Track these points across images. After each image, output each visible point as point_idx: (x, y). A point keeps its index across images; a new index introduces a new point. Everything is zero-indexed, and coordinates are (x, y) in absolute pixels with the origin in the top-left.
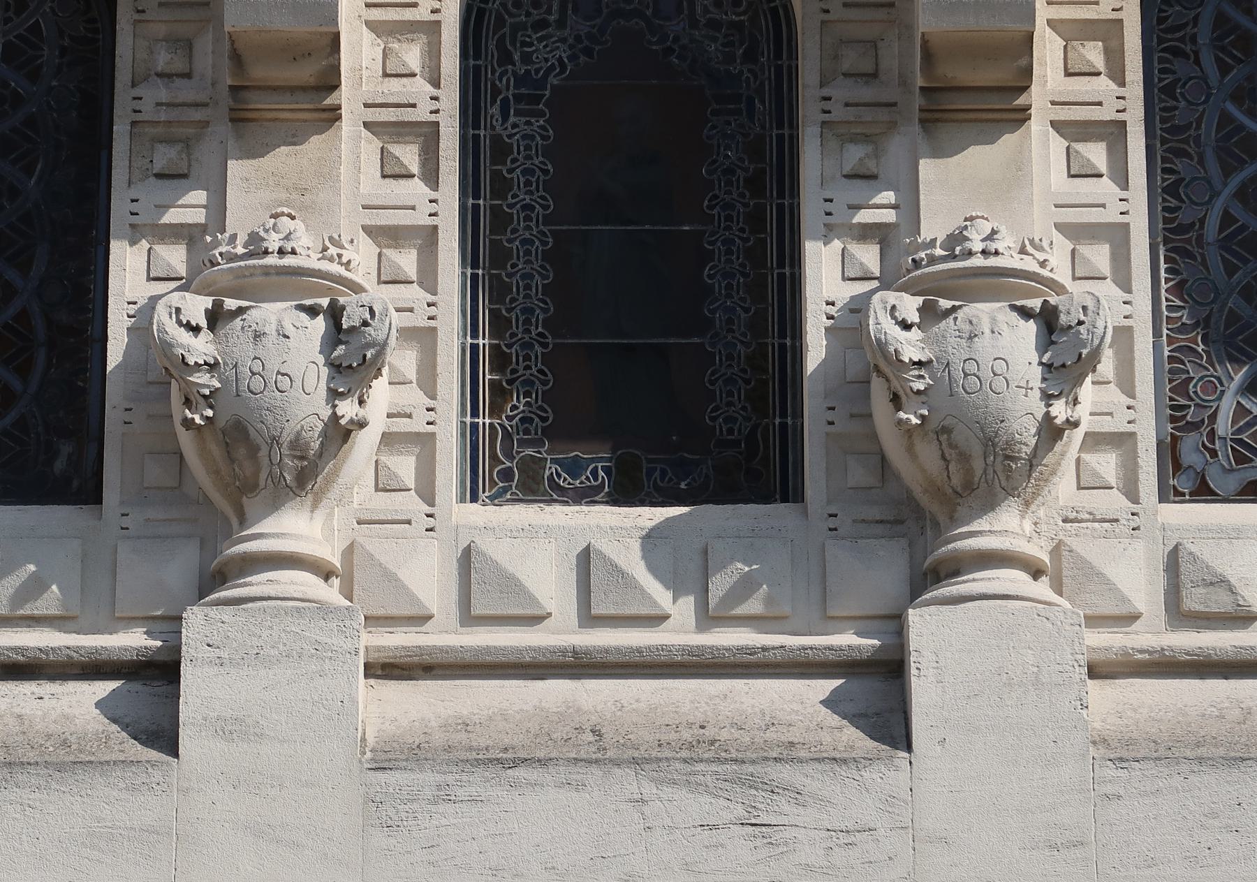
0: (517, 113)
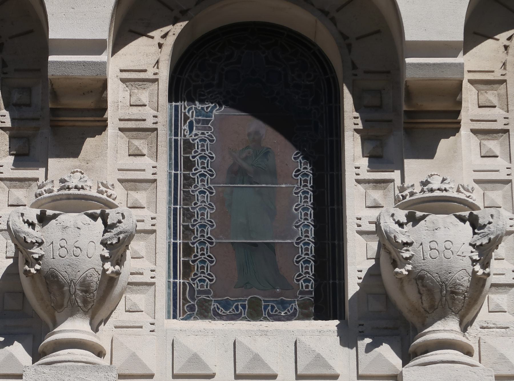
0: (197, 129)
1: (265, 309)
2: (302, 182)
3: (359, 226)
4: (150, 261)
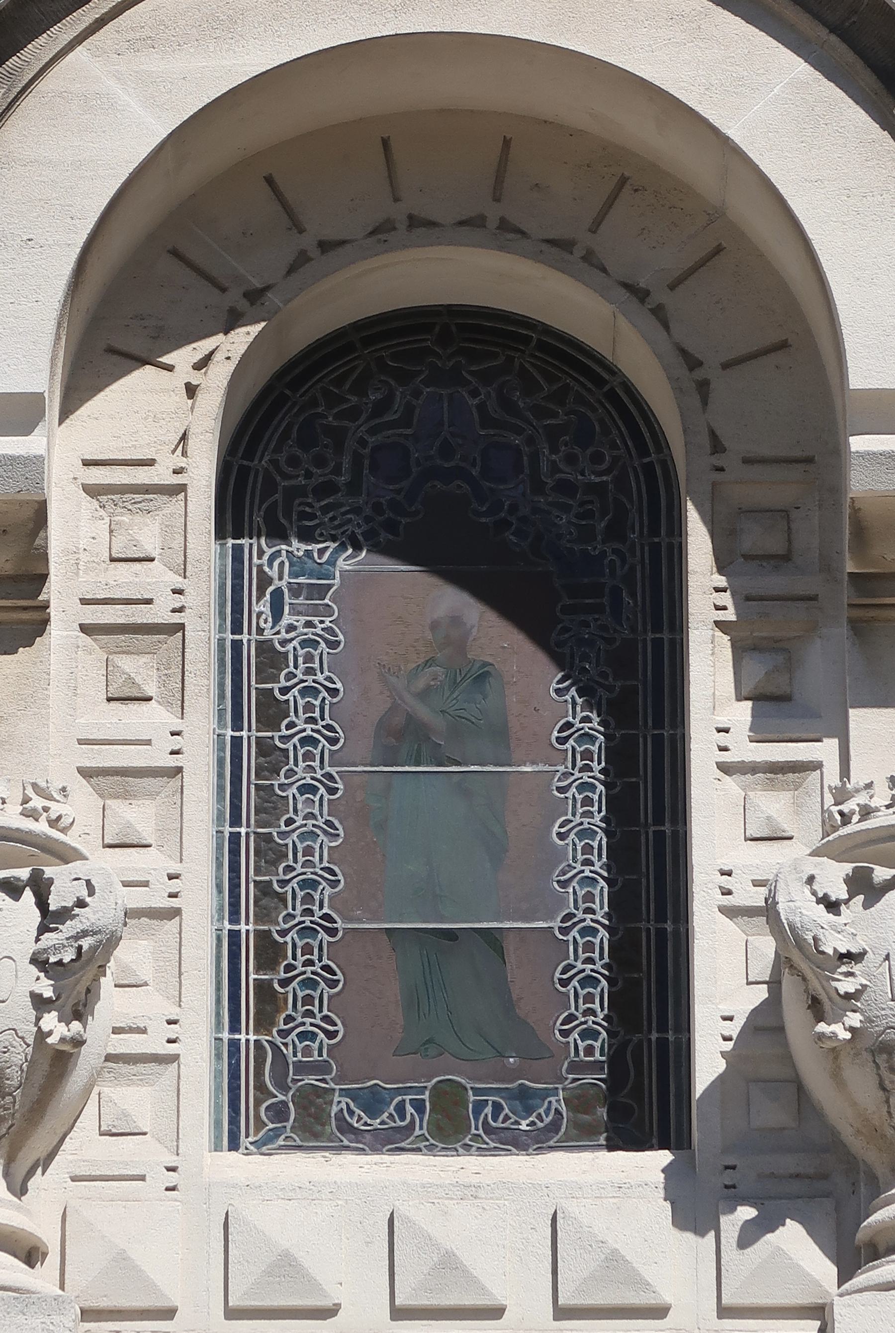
0: (295, 611)
1: (477, 1112)
2: (578, 757)
3: (727, 892)
4: (167, 994)
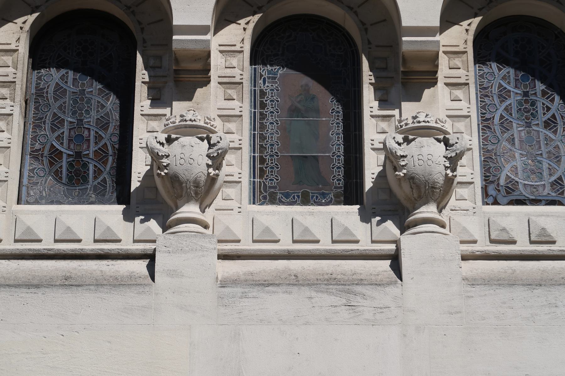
0: (268, 83)
3: (373, 145)
4: (238, 166)
